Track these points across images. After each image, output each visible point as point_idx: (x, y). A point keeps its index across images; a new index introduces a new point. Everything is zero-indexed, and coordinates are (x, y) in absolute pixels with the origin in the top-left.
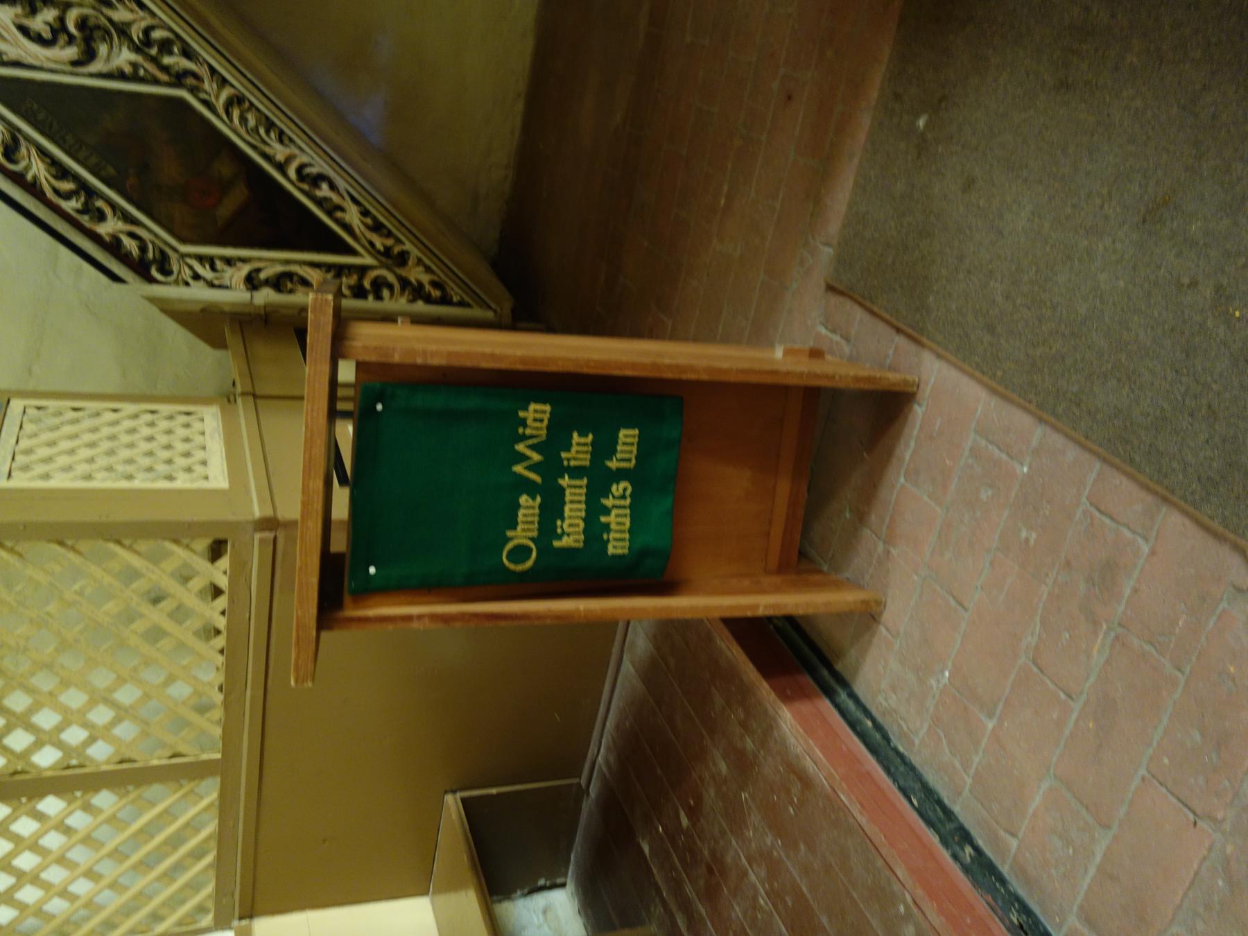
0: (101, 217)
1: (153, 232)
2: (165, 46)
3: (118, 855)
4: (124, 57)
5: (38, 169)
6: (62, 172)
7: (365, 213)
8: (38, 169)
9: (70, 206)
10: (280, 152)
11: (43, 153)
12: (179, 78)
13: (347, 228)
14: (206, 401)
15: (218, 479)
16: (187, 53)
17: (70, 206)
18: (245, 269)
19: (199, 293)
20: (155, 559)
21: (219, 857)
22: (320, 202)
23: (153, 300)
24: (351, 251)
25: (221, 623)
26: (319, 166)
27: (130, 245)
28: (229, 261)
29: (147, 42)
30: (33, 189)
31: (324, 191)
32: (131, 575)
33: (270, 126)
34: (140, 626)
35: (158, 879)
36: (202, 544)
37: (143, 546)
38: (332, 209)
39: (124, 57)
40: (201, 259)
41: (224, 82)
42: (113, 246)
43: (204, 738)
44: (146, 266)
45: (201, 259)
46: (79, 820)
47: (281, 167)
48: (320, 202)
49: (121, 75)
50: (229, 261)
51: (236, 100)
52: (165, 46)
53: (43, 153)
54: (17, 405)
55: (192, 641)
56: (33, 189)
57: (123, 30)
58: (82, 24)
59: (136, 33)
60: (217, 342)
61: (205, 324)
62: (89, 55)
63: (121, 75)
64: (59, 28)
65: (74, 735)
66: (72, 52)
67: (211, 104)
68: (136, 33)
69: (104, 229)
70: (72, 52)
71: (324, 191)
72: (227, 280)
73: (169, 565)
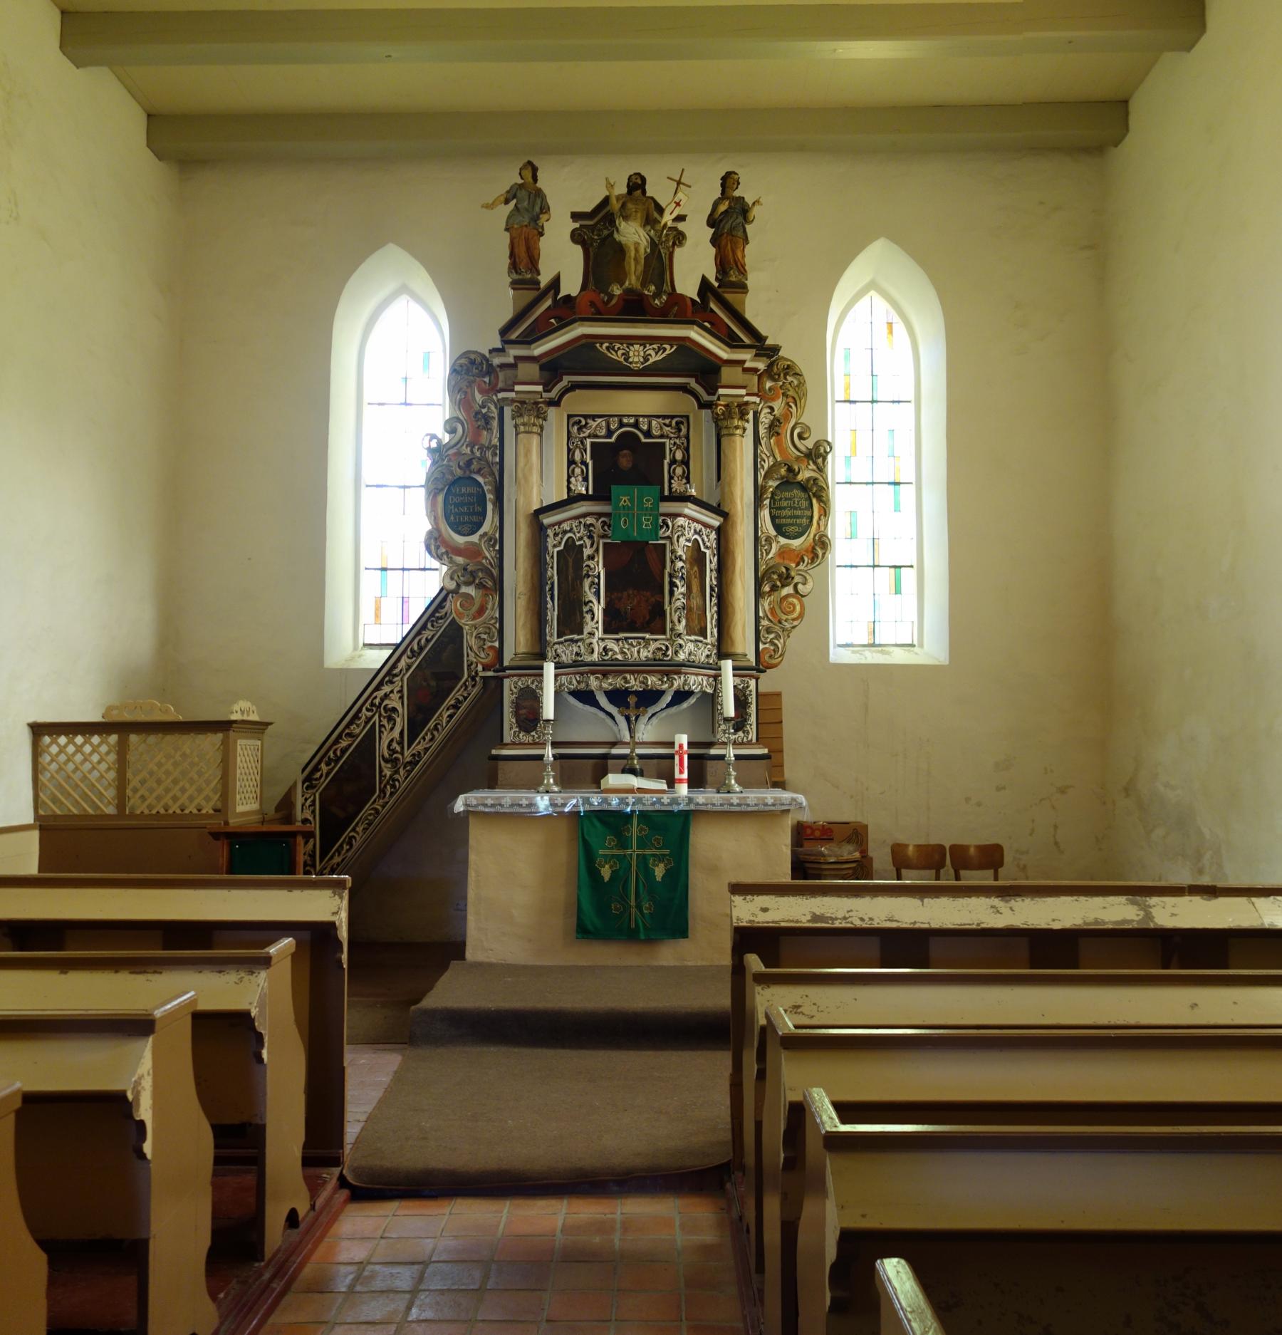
0: (327, 765)
1: (324, 783)
2: (393, 786)
3: (84, 778)
4: (388, 773)
5: (344, 744)
6: (344, 751)
7: (338, 864)
8: (344, 744)
9: (331, 754)
10: (360, 829)
11: (350, 746)
12: (383, 791)
13: (332, 858)
14: (261, 804)
15: (240, 809)
16: (392, 794)
17: (331, 754)
18: (311, 818)
19: (299, 800)
20: (215, 791)
21: (75, 815)
22: (341, 846)
23: (295, 783)
24: (321, 861)
25: (187, 811)
26: (355, 845)
27: (318, 775)
28: (313, 812)
29: (394, 780)
30: (336, 742)
31: (346, 847)
32: (208, 782)
33: (369, 824)
34: (187, 786)
35: (52, 793)
36: (219, 805)
37: (219, 786)
38: (339, 851)
39: (388, 773)
40: (314, 801)
41: (383, 807)
42: (316, 769)
43: (138, 805)
44: (309, 781)
45: (314, 801)
46: (103, 766)
47: (354, 830)
48: (341, 846)
49: (381, 771)
50: (313, 812)
51: (377, 811)
52: (393, 786)
53: (350, 746)
54: (259, 743)
55: (196, 802)
56: (336, 742)
57: (397, 772)
58: (397, 759)
59: (396, 776)
60: (278, 809)
61: (286, 804)
62: (386, 761)
63: (381, 771)
64: (394, 751)
65: (71, 749)
66: (387, 755)
67: (375, 802)
68: (396, 776)
69: (323, 765)
70: (387, 755)
71: (346, 847)
72: (305, 811)
73: (211, 794)
